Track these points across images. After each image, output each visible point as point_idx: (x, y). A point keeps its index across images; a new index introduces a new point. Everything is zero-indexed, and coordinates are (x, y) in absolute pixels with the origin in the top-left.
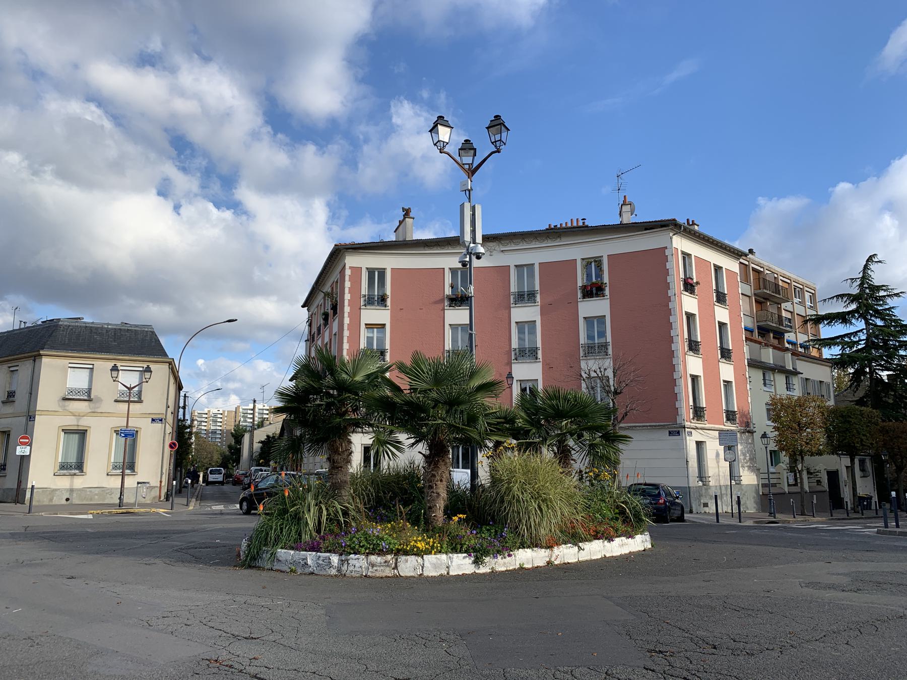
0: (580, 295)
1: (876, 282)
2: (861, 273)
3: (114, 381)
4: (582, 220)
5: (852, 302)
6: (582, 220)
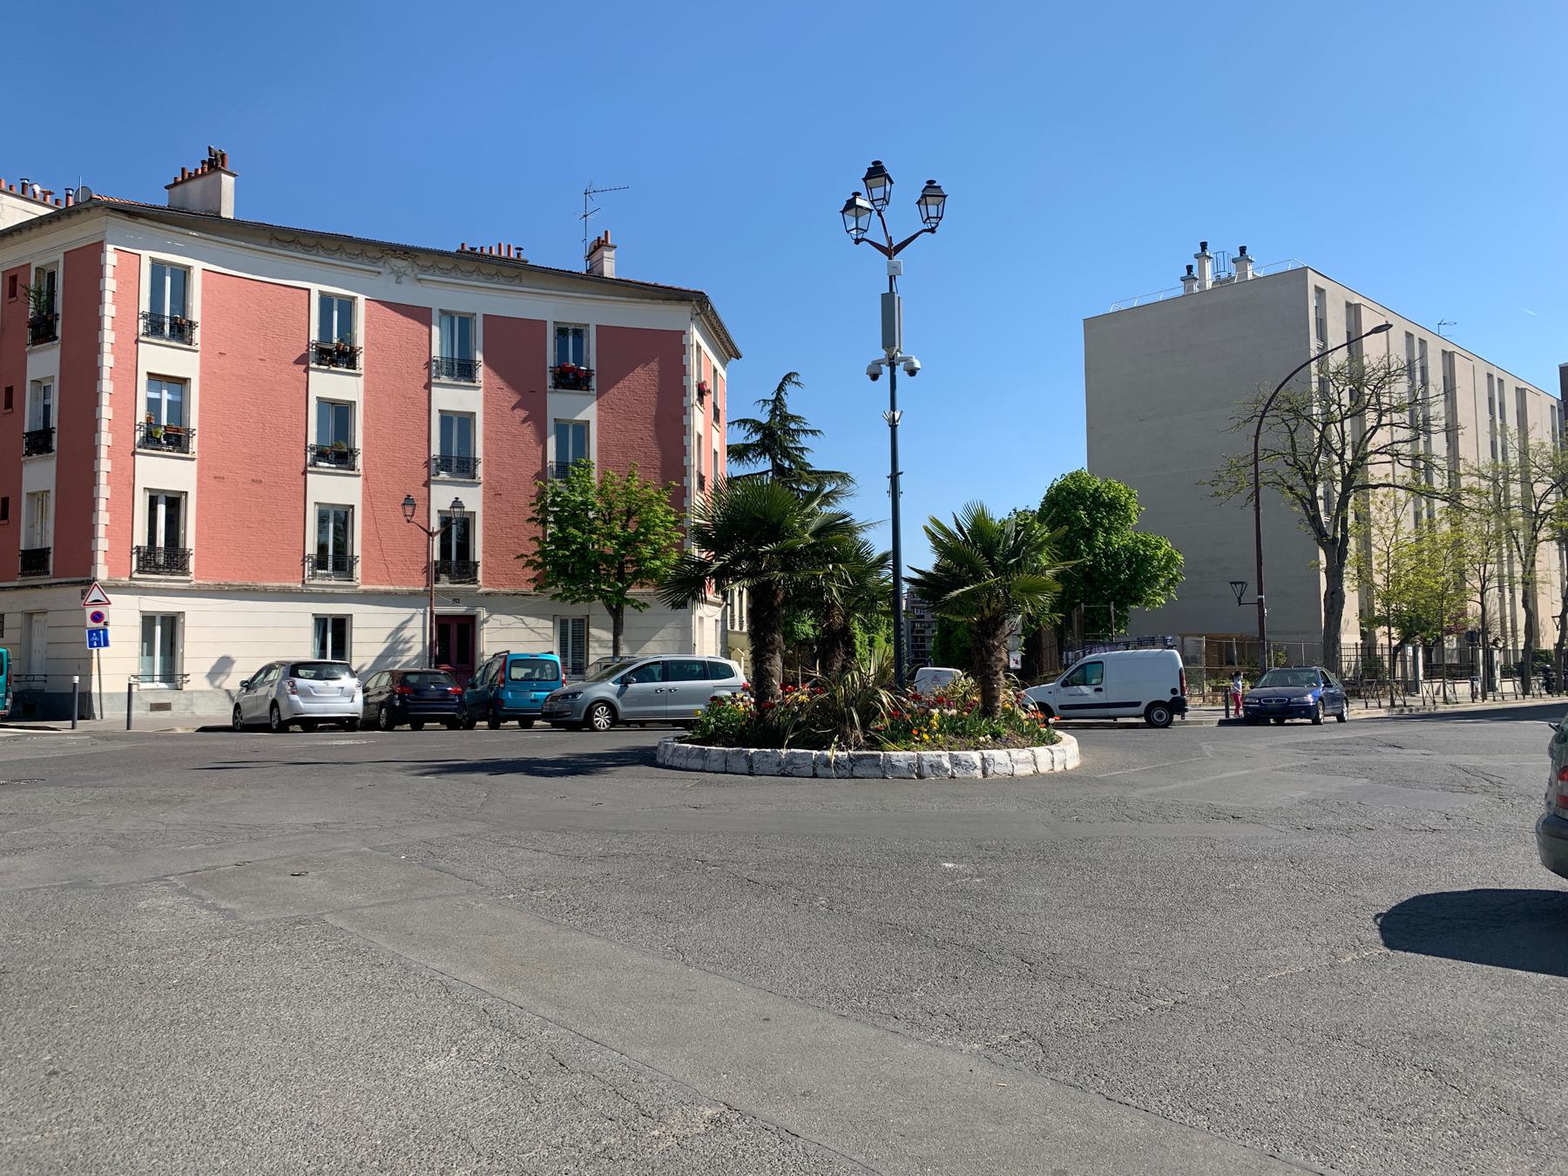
0: (550, 381)
1: (790, 410)
2: (775, 394)
3: (408, 521)
4: (517, 249)
5: (756, 432)
6: (517, 249)
